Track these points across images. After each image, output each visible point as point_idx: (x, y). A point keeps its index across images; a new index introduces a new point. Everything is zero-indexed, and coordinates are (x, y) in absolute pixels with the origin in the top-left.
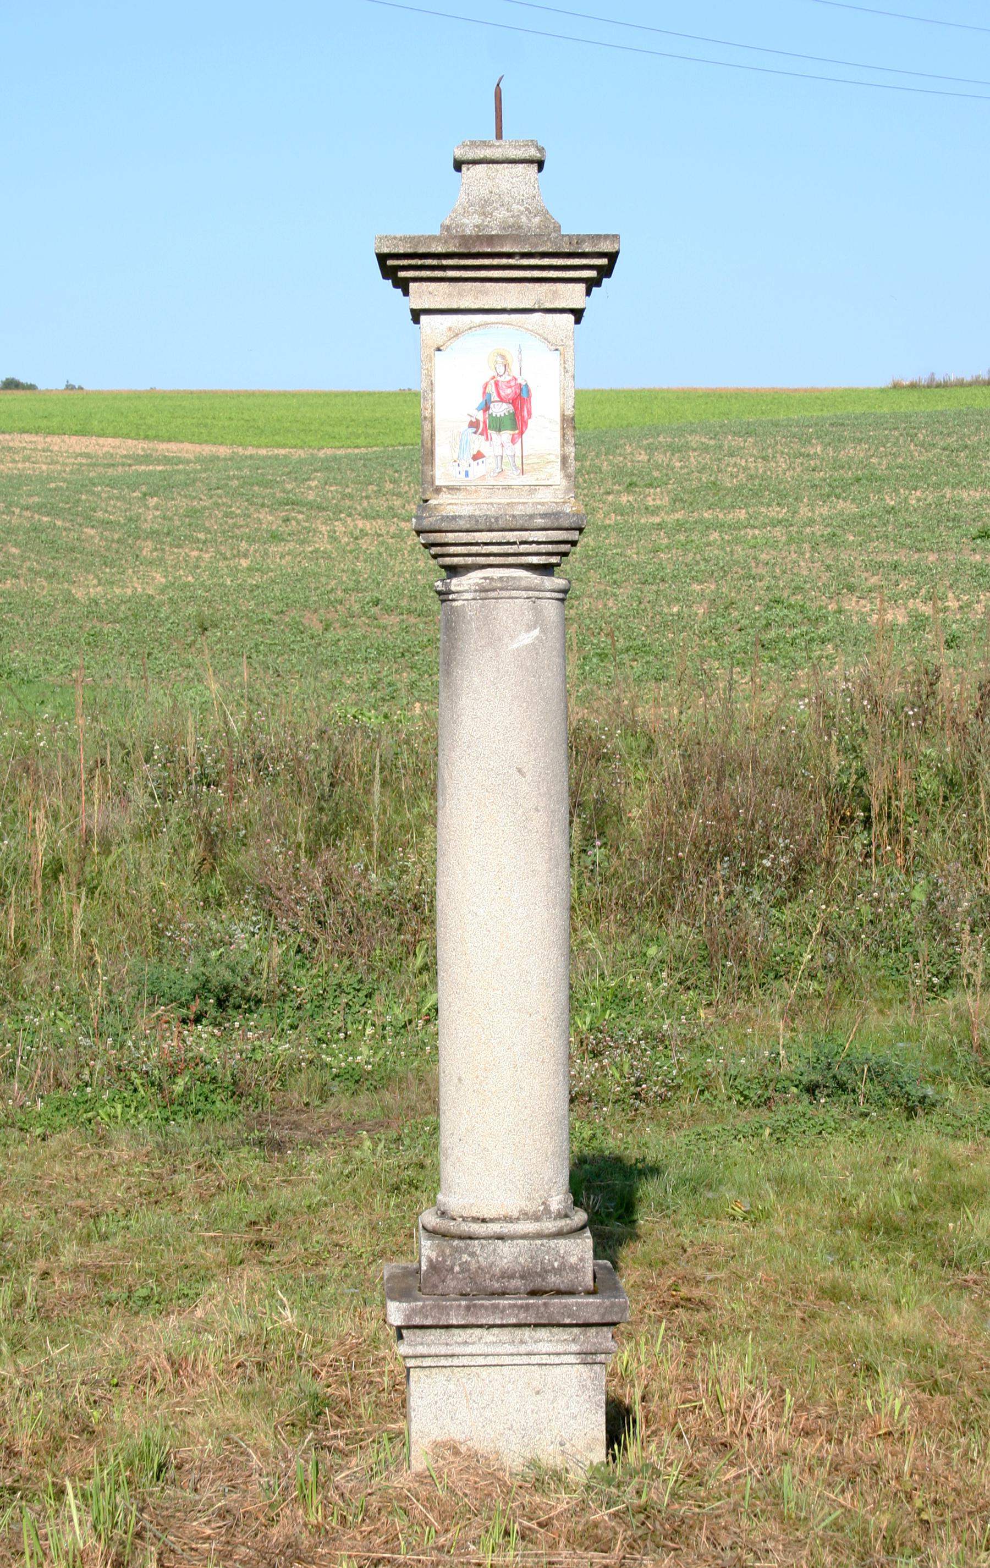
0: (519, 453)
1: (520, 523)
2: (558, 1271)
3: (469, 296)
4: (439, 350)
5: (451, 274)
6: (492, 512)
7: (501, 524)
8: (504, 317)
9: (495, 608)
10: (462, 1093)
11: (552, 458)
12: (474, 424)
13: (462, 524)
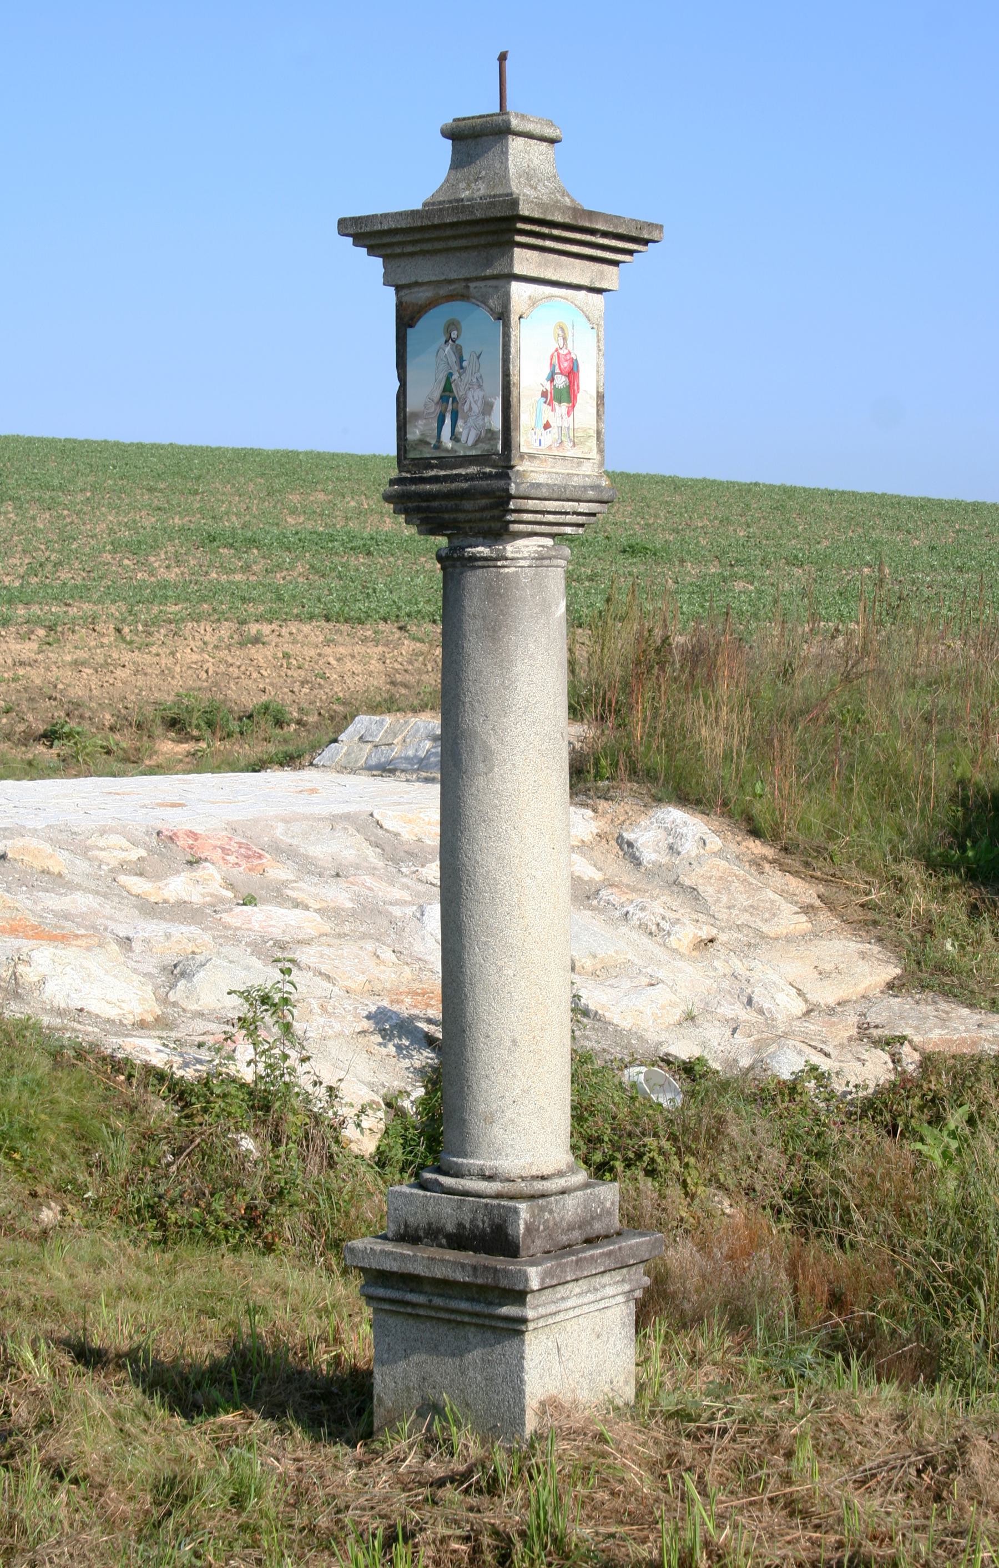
2: (599, 1217)
5: (548, 244)
7: (568, 495)
8: (563, 292)
9: (547, 576)
10: (517, 1055)
13: (544, 492)
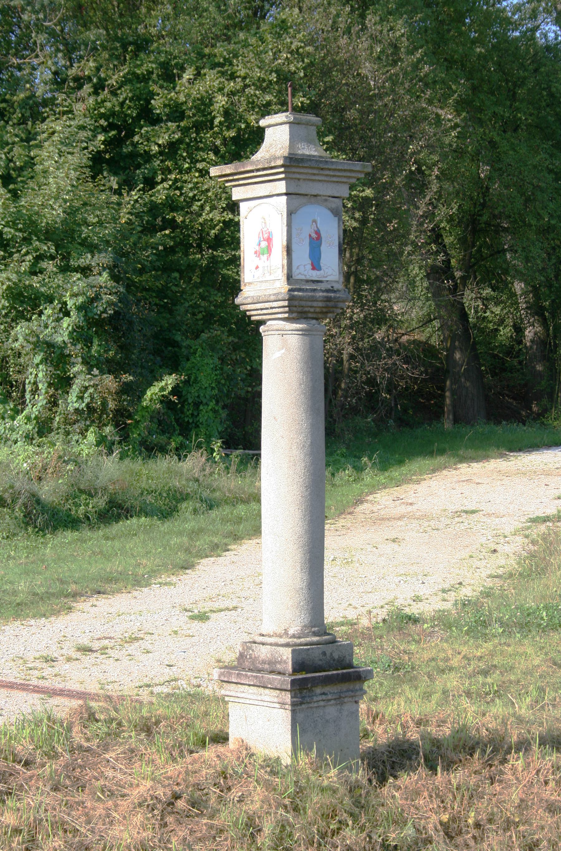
1: (266, 299)
2: (280, 663)
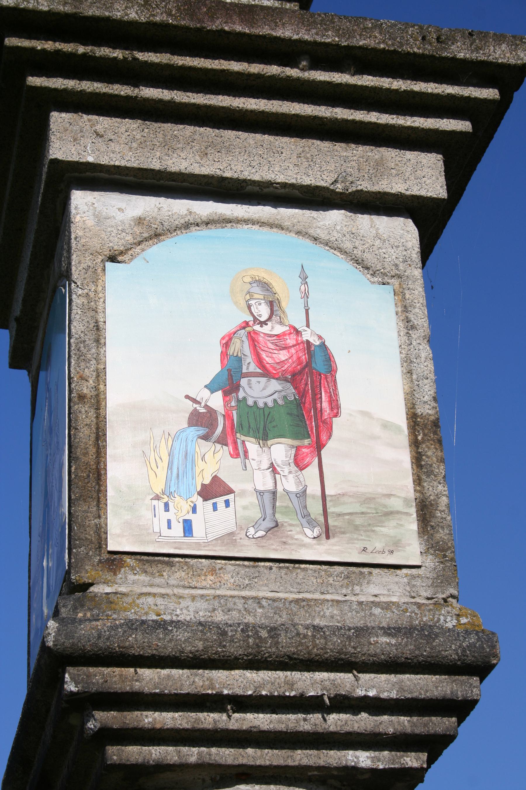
0: (314, 489)
3: (187, 151)
4: (113, 259)
6: (258, 616)
7: (286, 644)
11: (396, 504)
12: (202, 420)
